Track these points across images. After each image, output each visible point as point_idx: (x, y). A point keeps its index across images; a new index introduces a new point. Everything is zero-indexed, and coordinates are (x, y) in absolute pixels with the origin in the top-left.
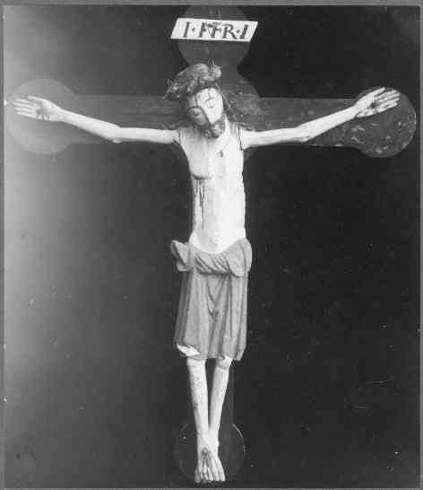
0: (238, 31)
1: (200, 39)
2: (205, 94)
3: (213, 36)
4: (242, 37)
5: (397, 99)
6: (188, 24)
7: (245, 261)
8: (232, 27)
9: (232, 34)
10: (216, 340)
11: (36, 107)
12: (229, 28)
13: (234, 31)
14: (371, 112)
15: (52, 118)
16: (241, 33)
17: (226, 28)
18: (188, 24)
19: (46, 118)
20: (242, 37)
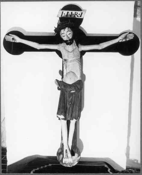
0: (79, 14)
1: (67, 17)
2: (70, 37)
3: (68, 12)
4: (81, 16)
5: (133, 36)
6: (63, 12)
7: (128, 148)
8: (77, 13)
9: (77, 15)
10: (66, 104)
11: (12, 38)
12: (76, 13)
13: (78, 15)
14: (124, 40)
15: (17, 42)
16: (80, 15)
17: (75, 14)
18: (63, 12)
19: (15, 42)
20: (81, 16)
